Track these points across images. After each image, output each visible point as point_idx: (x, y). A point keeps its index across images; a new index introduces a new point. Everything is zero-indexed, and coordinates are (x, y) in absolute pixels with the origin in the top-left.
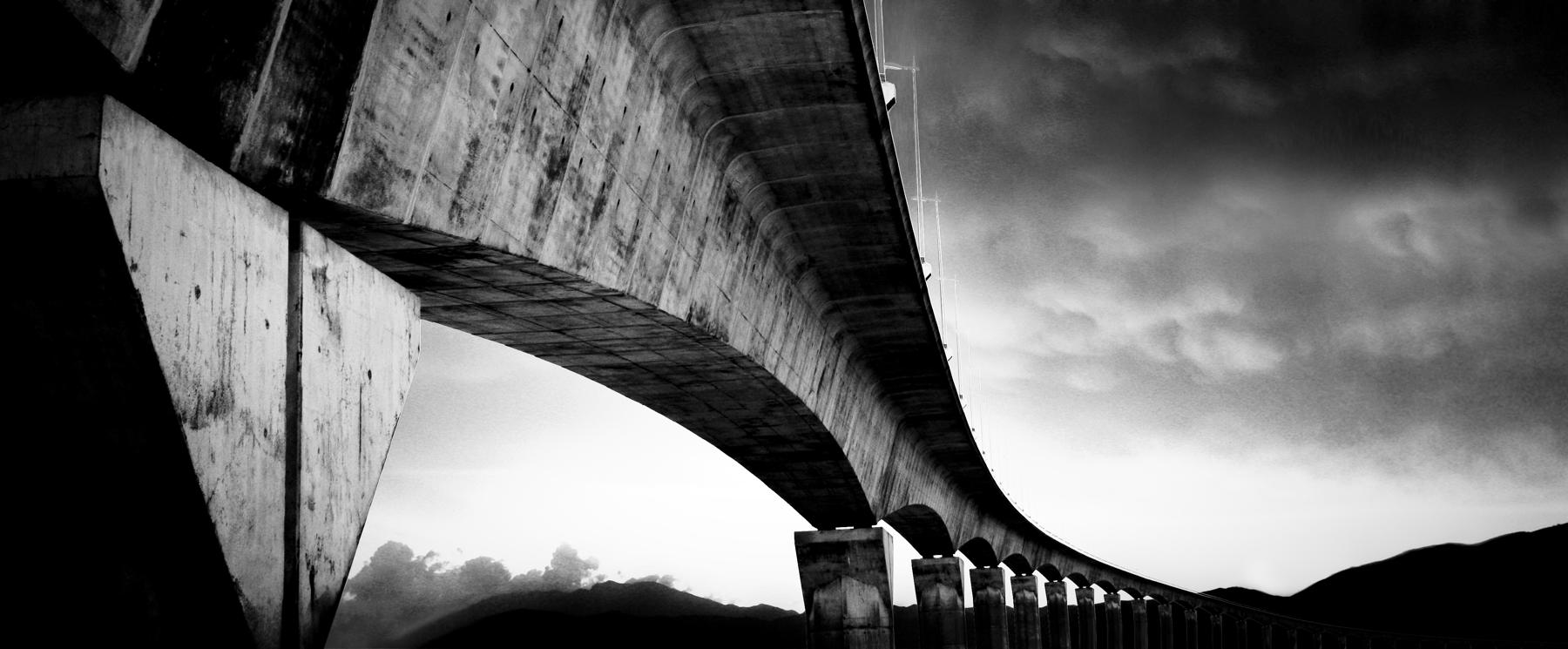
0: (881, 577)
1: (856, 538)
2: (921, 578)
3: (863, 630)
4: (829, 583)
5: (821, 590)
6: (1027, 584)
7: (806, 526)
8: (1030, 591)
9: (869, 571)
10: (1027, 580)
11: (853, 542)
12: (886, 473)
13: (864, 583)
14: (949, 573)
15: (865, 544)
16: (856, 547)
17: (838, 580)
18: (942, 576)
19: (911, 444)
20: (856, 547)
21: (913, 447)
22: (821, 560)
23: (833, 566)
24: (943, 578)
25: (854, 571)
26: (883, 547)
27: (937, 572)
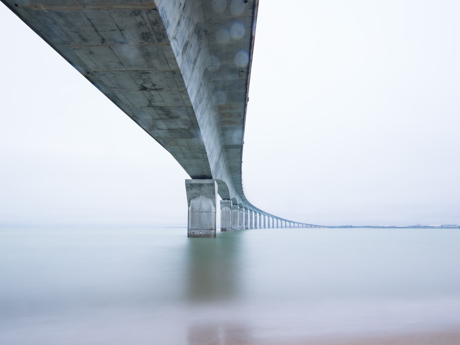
0: (213, 196)
1: (206, 183)
2: (222, 204)
3: (206, 213)
4: (196, 197)
5: (193, 199)
6: (241, 210)
7: (190, 178)
8: (242, 211)
9: (209, 194)
10: (242, 209)
11: (205, 183)
12: (217, 163)
13: (207, 198)
14: (228, 204)
15: (208, 185)
16: (206, 185)
17: (199, 196)
18: (227, 205)
19: (225, 160)
20: (206, 185)
21: (225, 161)
22: (194, 189)
23: (198, 192)
24: (227, 205)
25: (204, 194)
26: (214, 186)
27: (226, 203)
